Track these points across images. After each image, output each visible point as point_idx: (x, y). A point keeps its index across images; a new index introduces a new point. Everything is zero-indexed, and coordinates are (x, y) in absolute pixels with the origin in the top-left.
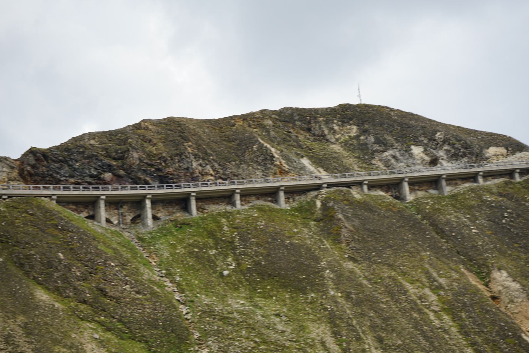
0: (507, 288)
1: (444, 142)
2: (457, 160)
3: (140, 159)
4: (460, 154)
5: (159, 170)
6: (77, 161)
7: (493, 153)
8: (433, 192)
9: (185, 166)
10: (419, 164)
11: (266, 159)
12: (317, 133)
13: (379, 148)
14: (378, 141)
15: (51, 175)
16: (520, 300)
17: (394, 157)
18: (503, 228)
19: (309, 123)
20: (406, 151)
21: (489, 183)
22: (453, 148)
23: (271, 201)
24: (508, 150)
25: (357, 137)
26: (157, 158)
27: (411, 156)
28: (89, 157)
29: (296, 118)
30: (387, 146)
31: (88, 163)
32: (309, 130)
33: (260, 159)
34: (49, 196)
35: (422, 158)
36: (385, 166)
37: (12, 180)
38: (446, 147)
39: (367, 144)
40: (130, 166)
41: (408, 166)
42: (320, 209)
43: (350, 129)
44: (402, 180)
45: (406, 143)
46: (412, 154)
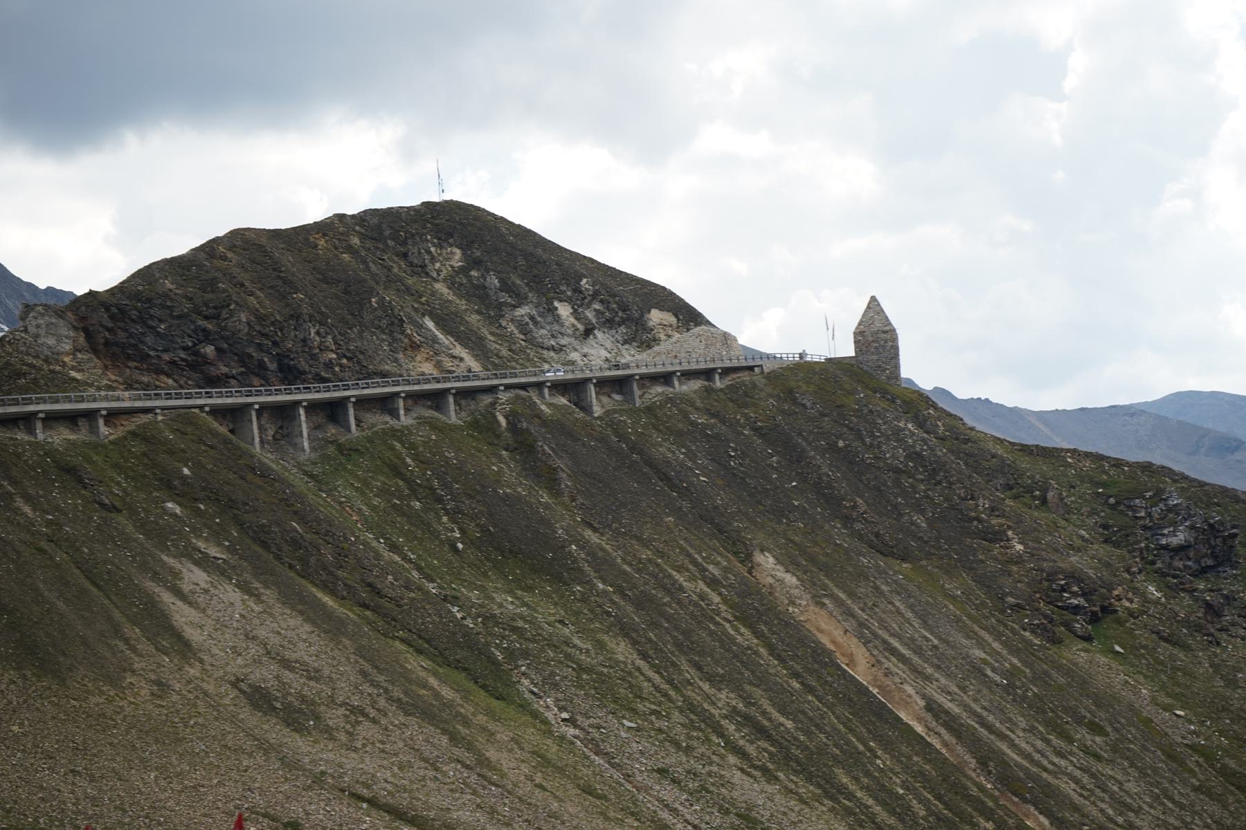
0: (781, 581)
1: (595, 295)
2: (611, 328)
3: (248, 324)
4: (617, 319)
5: (275, 343)
6: (161, 321)
7: (658, 321)
8: (618, 397)
9: (301, 336)
10: (569, 336)
11: (392, 324)
12: (416, 261)
13: (509, 300)
14: (506, 287)
15: (134, 345)
16: (804, 603)
17: (532, 318)
18: (735, 475)
19: (404, 243)
20: (549, 310)
21: (684, 388)
22: (608, 308)
23: (431, 408)
24: (678, 320)
25: (464, 270)
26: (268, 322)
27: (557, 319)
28: (179, 317)
29: (387, 233)
30: (521, 300)
31: (179, 326)
32: (405, 256)
33: (384, 323)
34: (201, 407)
35: (573, 325)
36: (521, 332)
37: (80, 351)
38: (597, 306)
39: (485, 288)
40: (234, 334)
41: (553, 336)
42: (507, 429)
43: (452, 253)
44: (587, 381)
45: (544, 295)
46: (558, 316)
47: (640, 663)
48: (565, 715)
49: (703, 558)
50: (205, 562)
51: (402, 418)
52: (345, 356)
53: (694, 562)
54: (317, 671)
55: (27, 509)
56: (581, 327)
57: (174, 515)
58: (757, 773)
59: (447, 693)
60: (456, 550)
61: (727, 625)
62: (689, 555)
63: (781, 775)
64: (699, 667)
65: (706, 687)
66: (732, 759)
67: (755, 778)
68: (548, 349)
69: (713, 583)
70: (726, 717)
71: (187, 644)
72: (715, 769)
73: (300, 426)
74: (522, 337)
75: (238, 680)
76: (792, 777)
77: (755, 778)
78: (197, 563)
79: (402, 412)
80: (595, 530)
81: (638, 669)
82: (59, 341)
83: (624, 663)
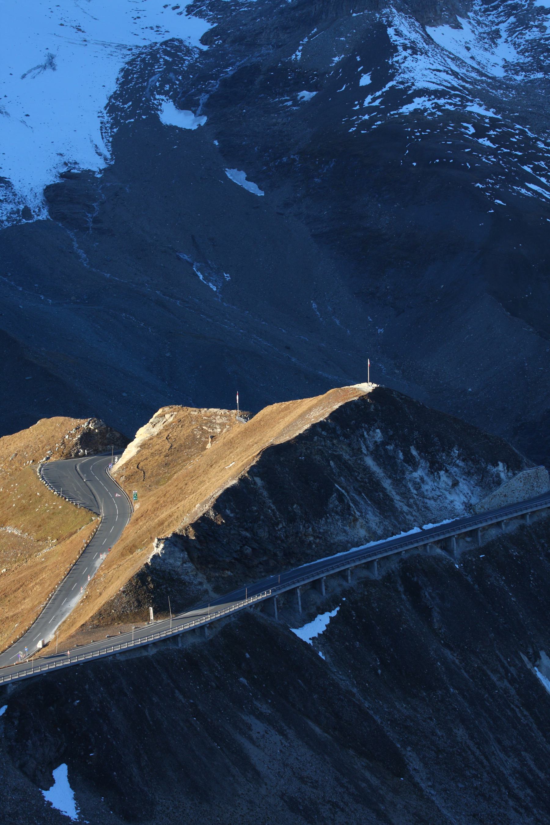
47: (471, 744)
48: (430, 784)
49: (508, 662)
50: (260, 716)
51: (350, 581)
52: (318, 537)
53: (503, 666)
54: (317, 782)
55: (181, 697)
56: (450, 483)
57: (243, 686)
58: (522, 811)
59: (375, 781)
60: (377, 674)
61: (517, 710)
62: (500, 661)
63: (535, 811)
64: (499, 742)
65: (502, 755)
66: (511, 803)
67: (521, 813)
68: (429, 499)
69: (512, 681)
70: (510, 775)
71: (258, 773)
72: (502, 811)
73: (297, 599)
74: (415, 492)
75: (283, 794)
76: (540, 811)
77: (521, 813)
78: (258, 718)
79: (349, 578)
80: (451, 649)
81: (468, 746)
82: (176, 561)
83: (461, 743)
